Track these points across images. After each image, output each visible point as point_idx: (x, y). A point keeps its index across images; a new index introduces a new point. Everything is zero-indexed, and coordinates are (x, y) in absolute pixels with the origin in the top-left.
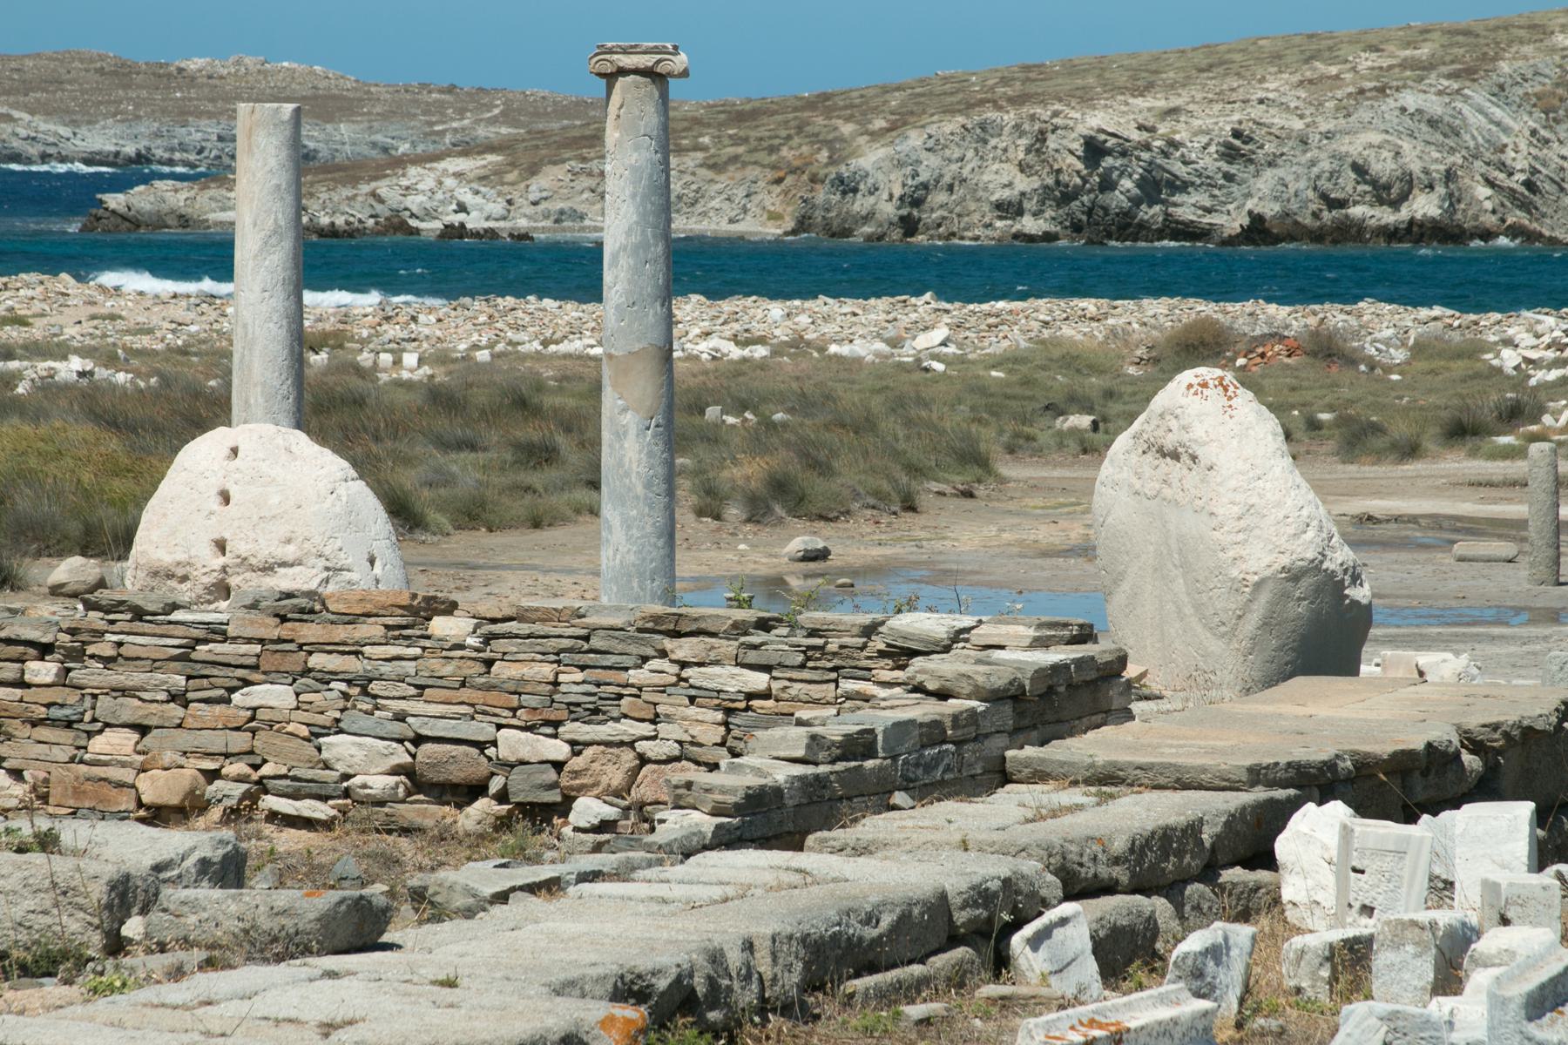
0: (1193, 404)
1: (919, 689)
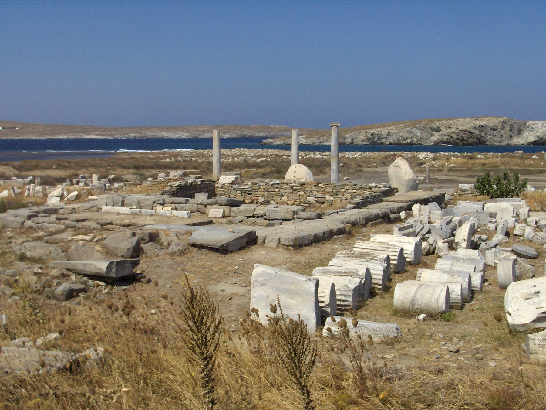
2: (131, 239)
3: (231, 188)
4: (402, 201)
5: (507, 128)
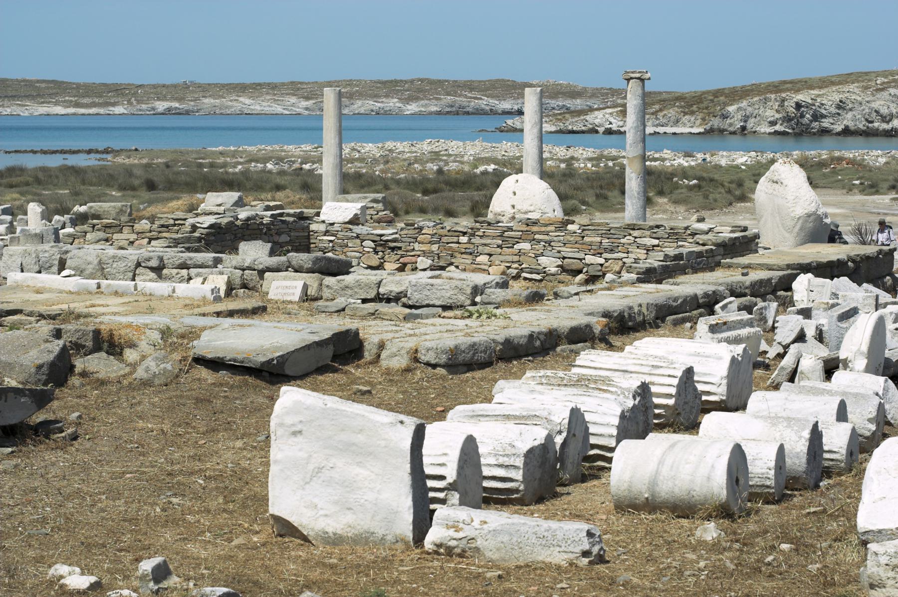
1: (698, 243)
2: (48, 345)
3: (349, 234)
4: (770, 268)
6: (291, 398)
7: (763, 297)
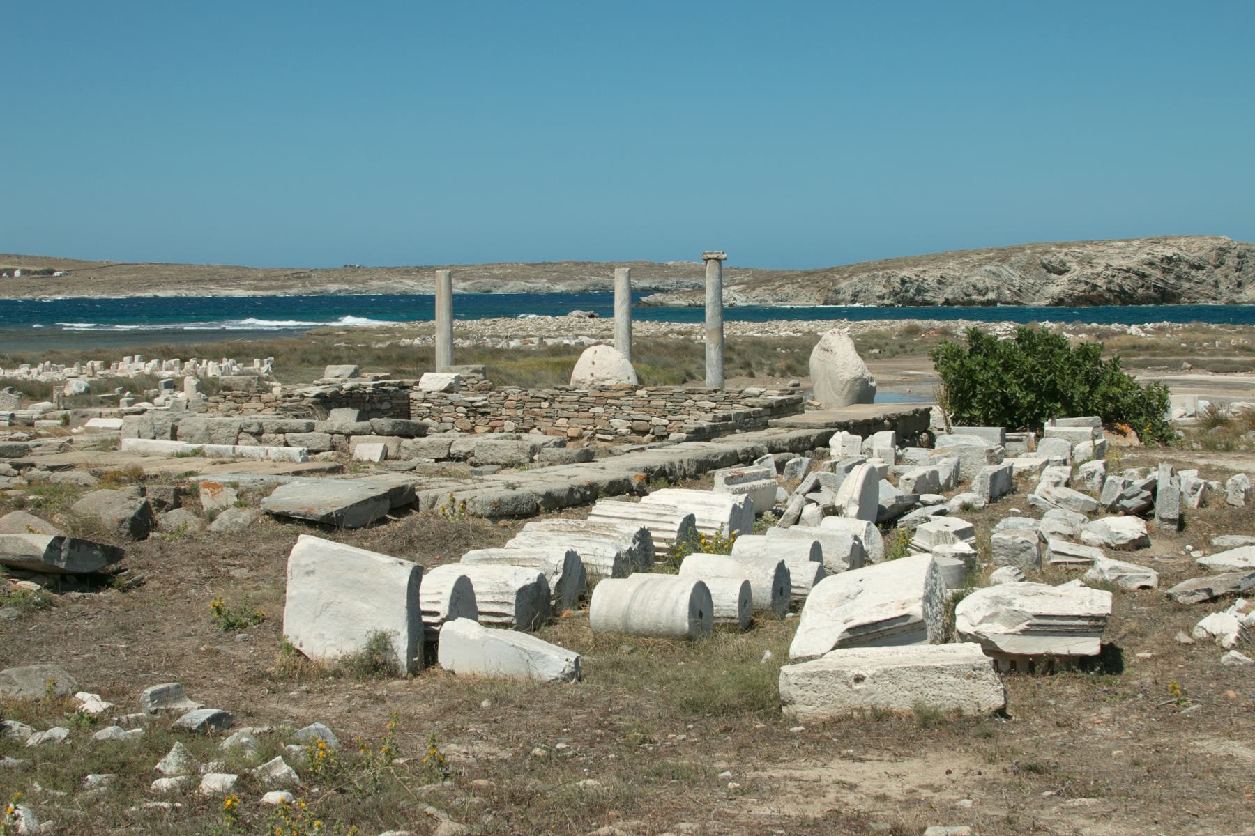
0: (831, 338)
5: (1231, 261)
6: (307, 544)
7: (802, 453)
